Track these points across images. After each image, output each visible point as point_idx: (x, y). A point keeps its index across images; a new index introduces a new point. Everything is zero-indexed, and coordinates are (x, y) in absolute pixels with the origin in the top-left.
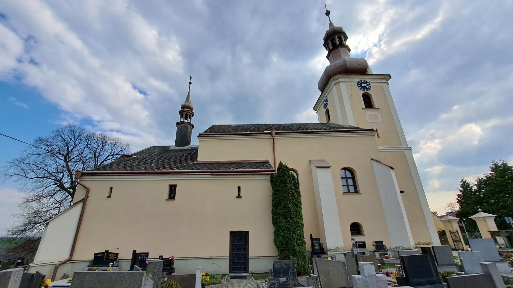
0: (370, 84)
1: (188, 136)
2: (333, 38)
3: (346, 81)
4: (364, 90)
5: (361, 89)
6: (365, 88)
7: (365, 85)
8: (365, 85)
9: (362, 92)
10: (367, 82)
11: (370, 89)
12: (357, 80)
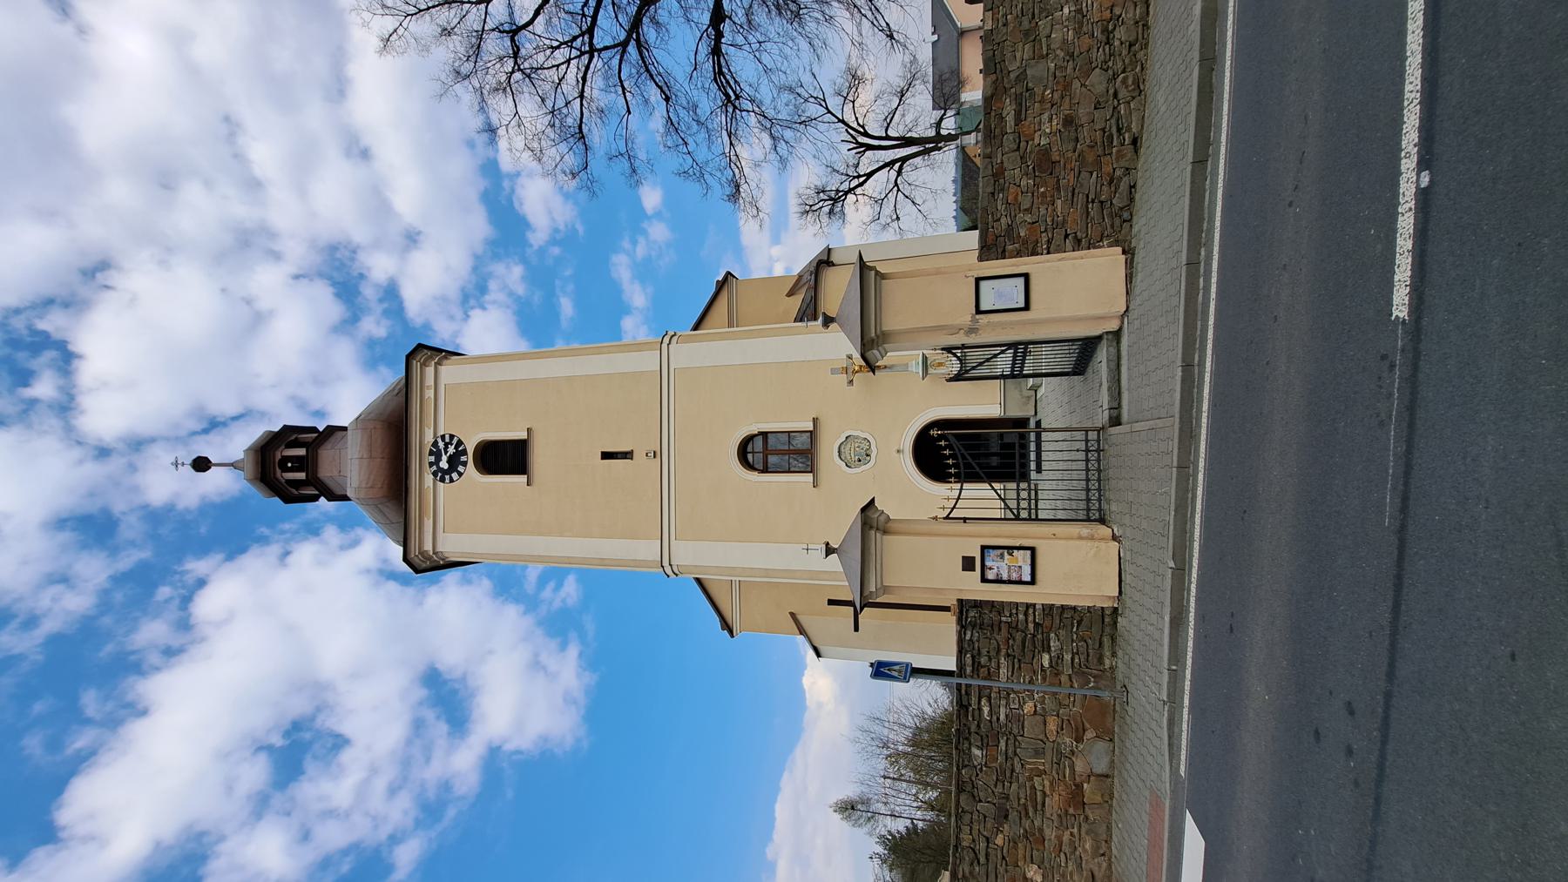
0: (443, 437)
1: (1388, 770)
2: (280, 460)
3: (433, 383)
4: (465, 464)
5: (460, 474)
6: (454, 462)
7: (444, 458)
8: (444, 458)
9: (471, 470)
10: (435, 444)
11: (460, 443)
12: (429, 479)
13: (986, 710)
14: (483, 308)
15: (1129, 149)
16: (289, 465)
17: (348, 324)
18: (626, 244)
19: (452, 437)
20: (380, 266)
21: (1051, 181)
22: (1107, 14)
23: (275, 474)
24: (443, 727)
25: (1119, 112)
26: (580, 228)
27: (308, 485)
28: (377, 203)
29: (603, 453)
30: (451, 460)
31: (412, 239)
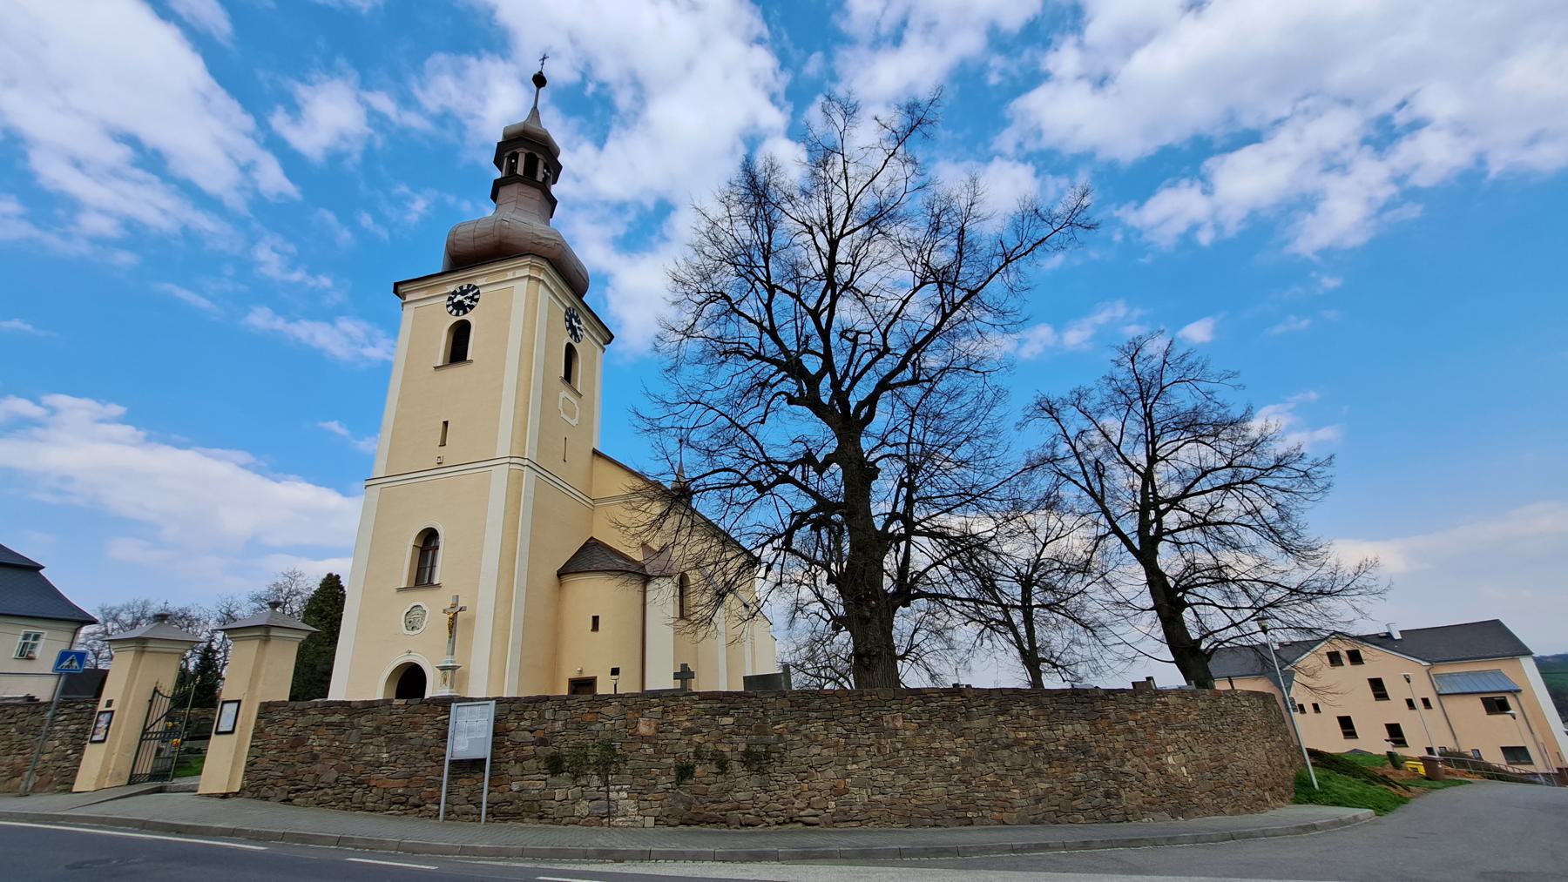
4: (457, 315)
6: (460, 306)
10: (475, 287)
11: (472, 307)
13: (61, 718)
14: (1037, 175)
15: (284, 796)
16: (513, 161)
17: (998, 41)
18: (1138, 312)
19: (477, 300)
20: (1065, 60)
21: (286, 747)
22: (373, 783)
23: (506, 151)
24: (621, 230)
25: (310, 790)
26: (1146, 260)
27: (510, 173)
28: (1134, 39)
29: (598, 617)
30: (461, 302)
31: (1101, 82)
